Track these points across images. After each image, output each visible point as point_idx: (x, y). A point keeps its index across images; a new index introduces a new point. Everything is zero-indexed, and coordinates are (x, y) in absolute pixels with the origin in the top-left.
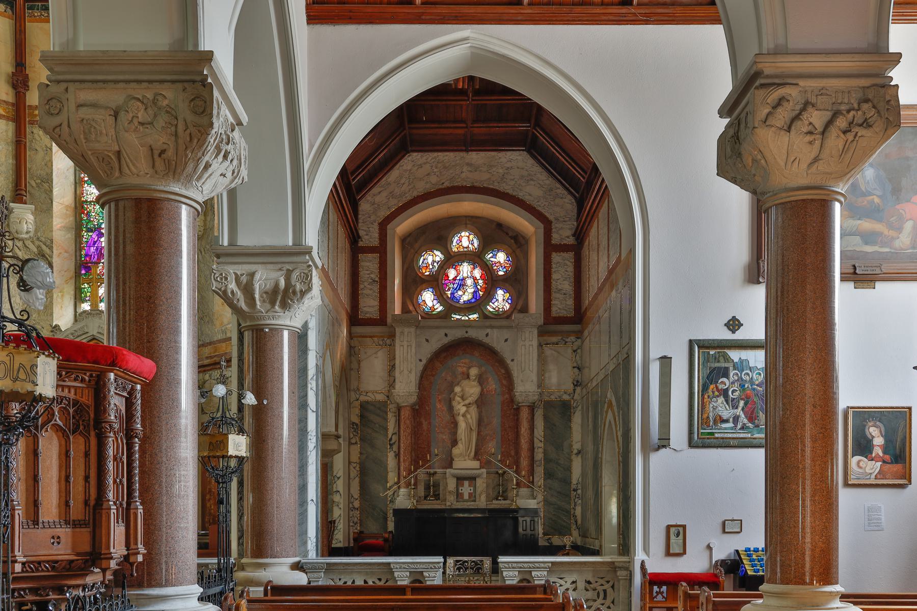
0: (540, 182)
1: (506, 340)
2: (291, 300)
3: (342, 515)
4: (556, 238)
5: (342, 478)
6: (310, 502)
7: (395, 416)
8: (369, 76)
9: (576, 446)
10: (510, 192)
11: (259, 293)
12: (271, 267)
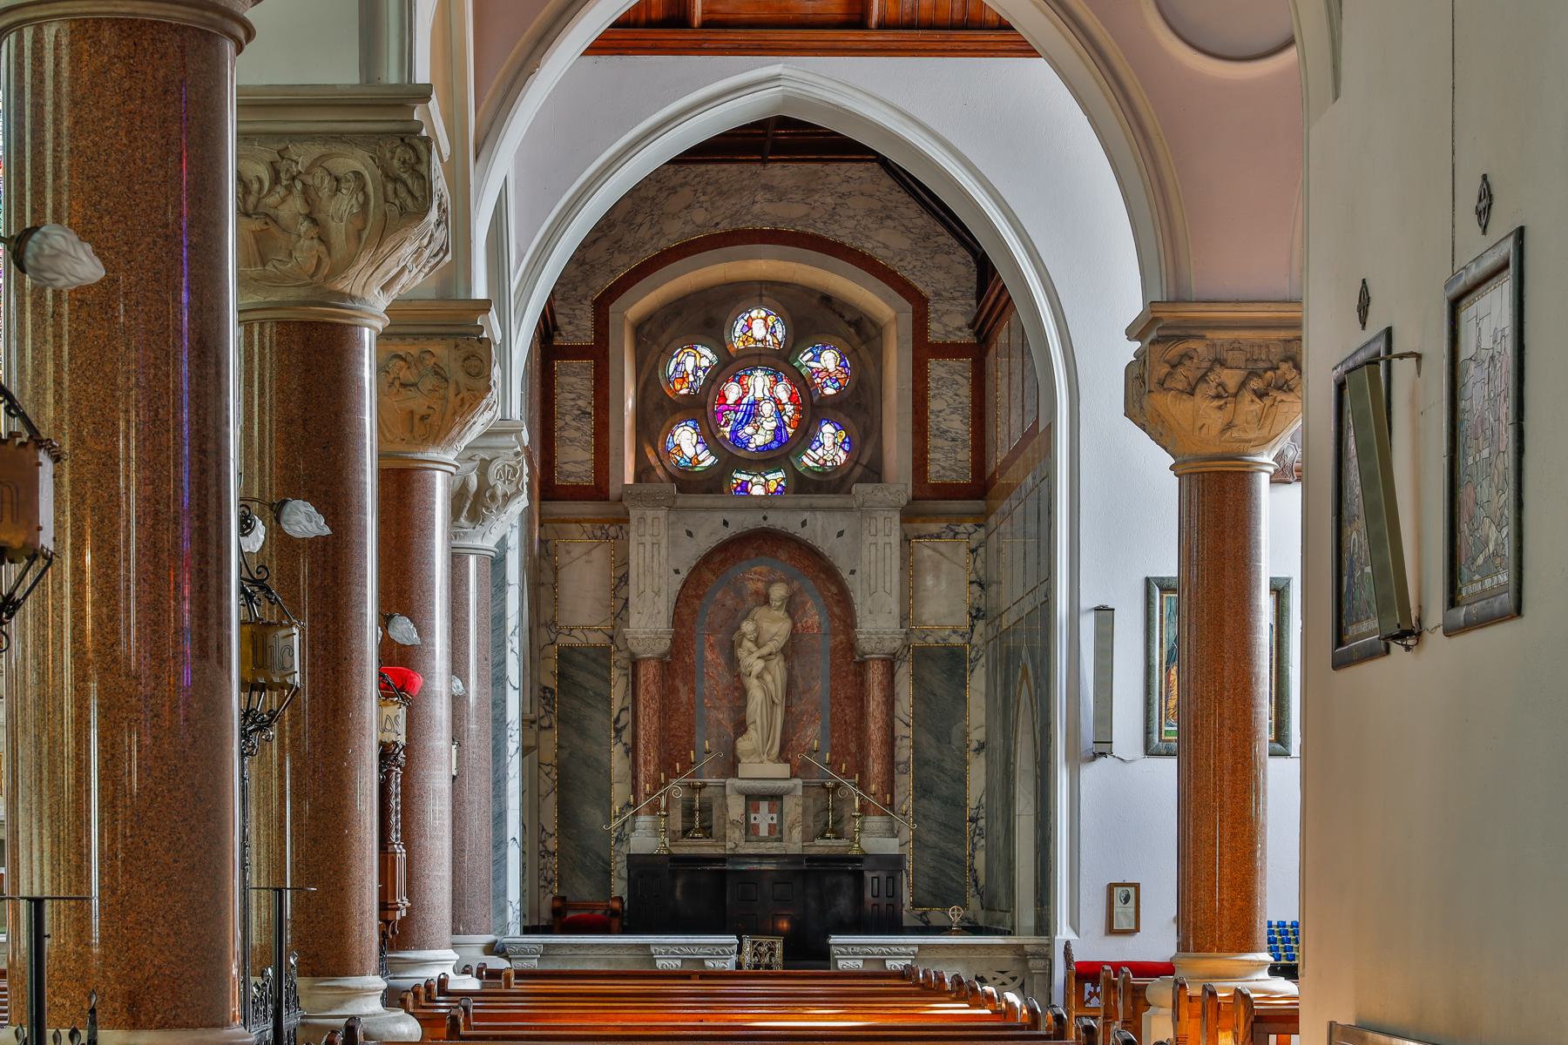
0: (906, 222)
1: (840, 534)
2: (487, 508)
4: (936, 331)
6: (510, 842)
7: (627, 675)
8: (615, 141)
9: (977, 735)
10: (848, 241)
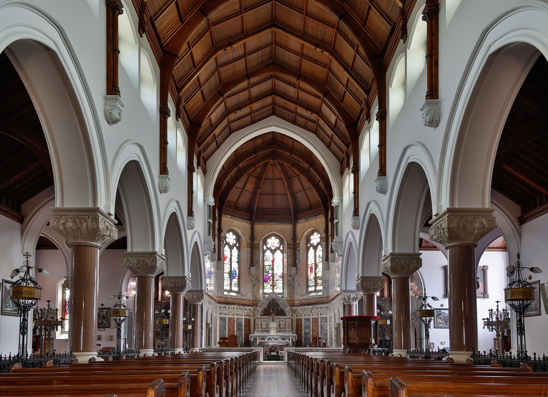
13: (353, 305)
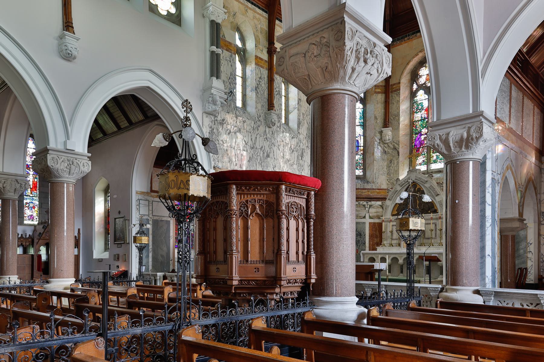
2: (471, 144)
3: (533, 265)
5: (533, 245)
11: (453, 143)
12: (458, 127)
13: (465, 162)
